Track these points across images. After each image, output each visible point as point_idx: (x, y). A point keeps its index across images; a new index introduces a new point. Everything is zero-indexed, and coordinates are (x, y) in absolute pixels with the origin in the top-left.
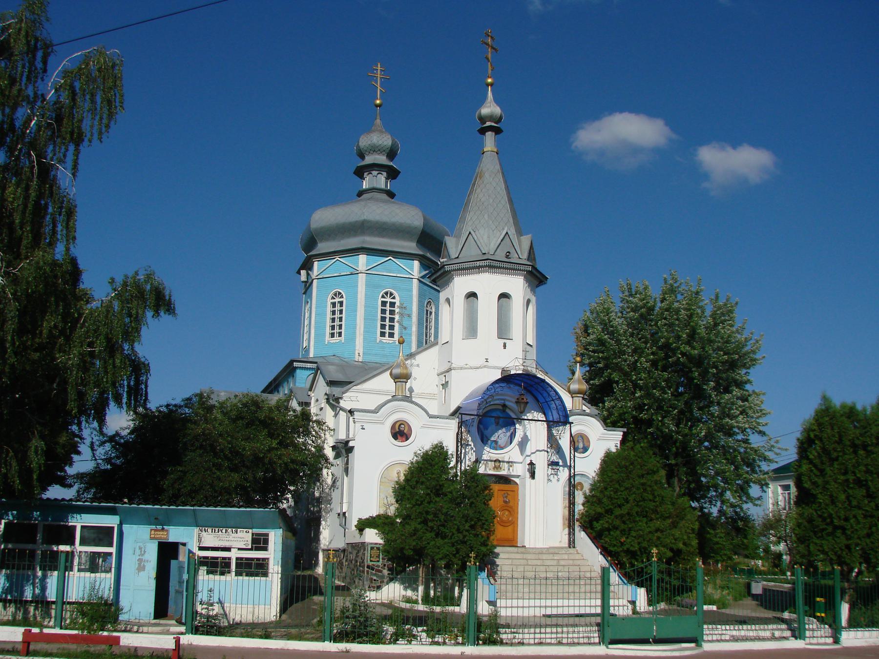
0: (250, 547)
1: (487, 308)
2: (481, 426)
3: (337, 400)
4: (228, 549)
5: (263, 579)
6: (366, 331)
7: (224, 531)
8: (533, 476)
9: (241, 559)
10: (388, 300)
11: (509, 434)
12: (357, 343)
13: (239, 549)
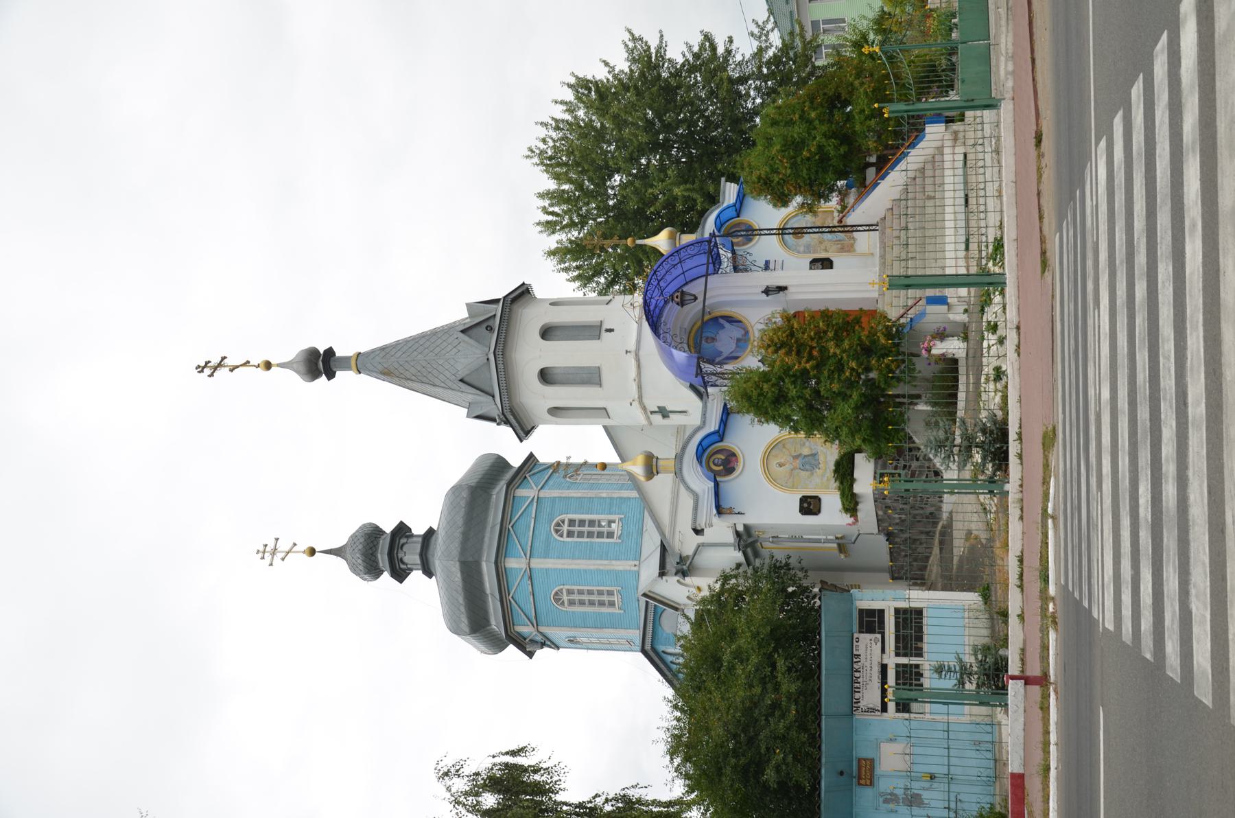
0: (879, 636)
1: (561, 354)
2: (718, 360)
3: (682, 559)
4: (884, 668)
5: (925, 614)
6: (604, 555)
7: (857, 675)
8: (782, 289)
9: (897, 648)
10: (565, 528)
11: (727, 325)
12: (621, 568)
13: (883, 650)
